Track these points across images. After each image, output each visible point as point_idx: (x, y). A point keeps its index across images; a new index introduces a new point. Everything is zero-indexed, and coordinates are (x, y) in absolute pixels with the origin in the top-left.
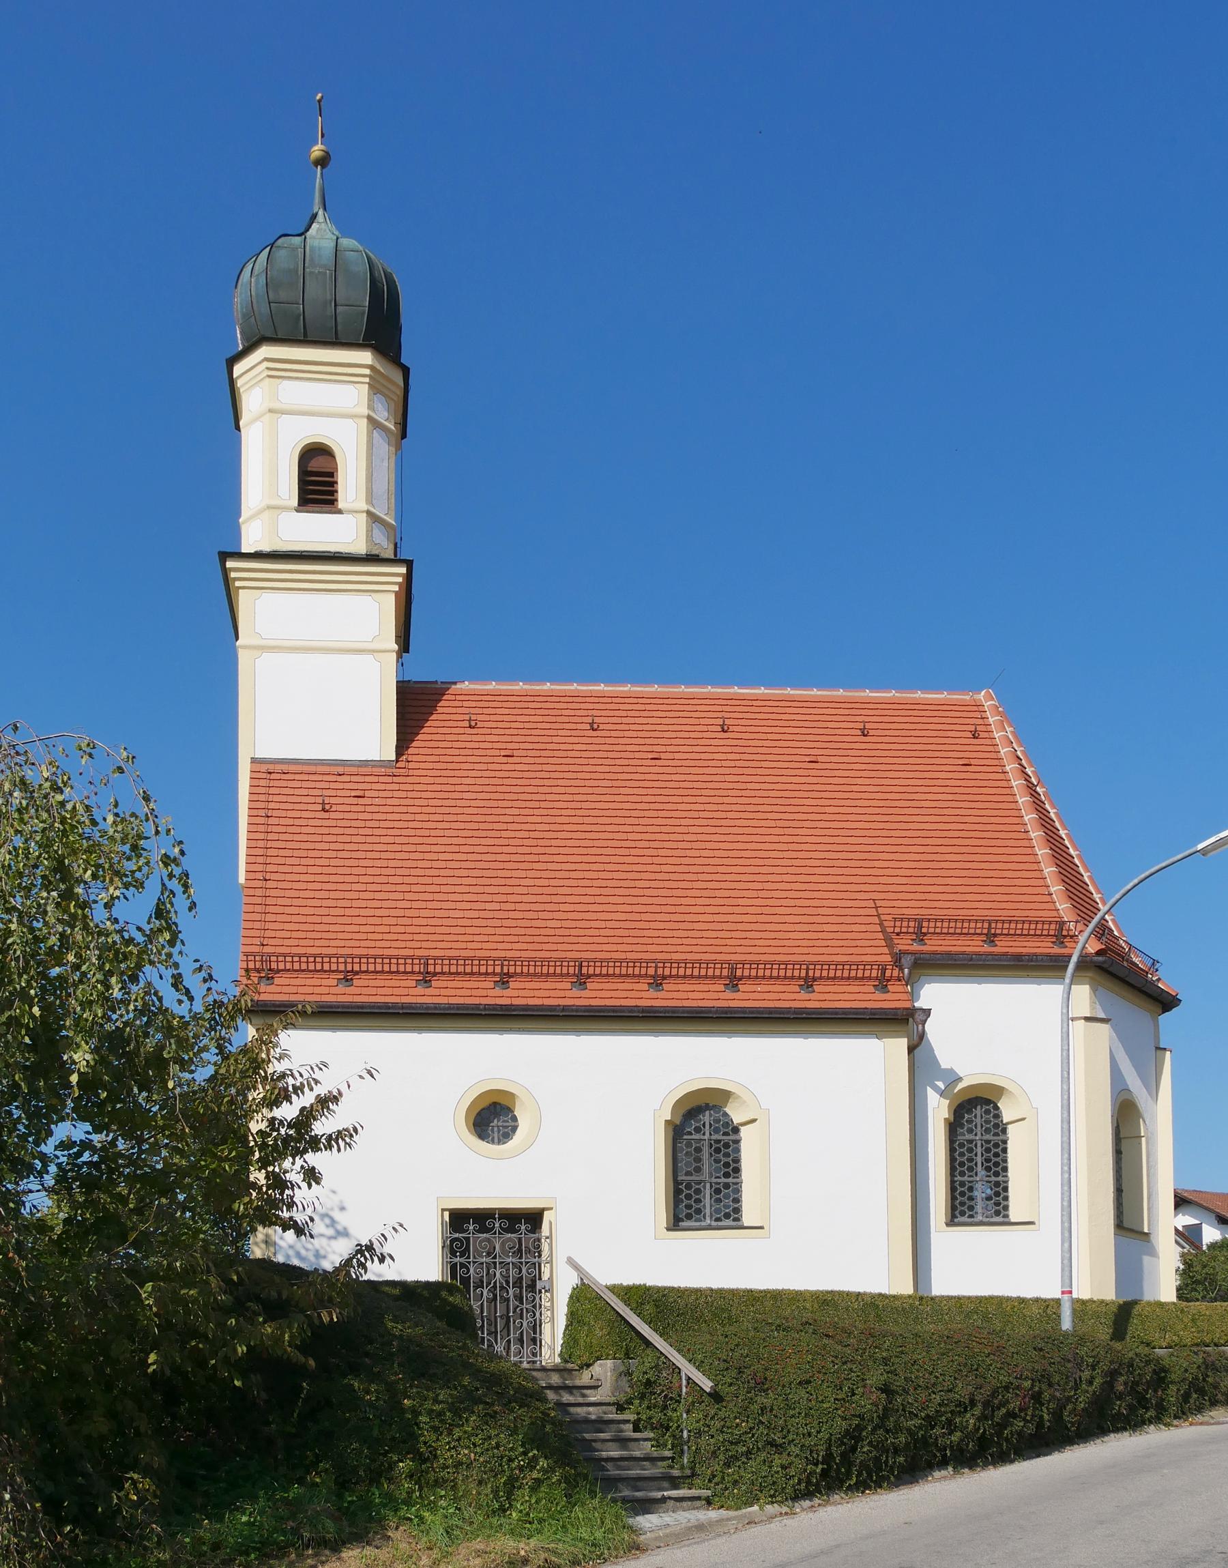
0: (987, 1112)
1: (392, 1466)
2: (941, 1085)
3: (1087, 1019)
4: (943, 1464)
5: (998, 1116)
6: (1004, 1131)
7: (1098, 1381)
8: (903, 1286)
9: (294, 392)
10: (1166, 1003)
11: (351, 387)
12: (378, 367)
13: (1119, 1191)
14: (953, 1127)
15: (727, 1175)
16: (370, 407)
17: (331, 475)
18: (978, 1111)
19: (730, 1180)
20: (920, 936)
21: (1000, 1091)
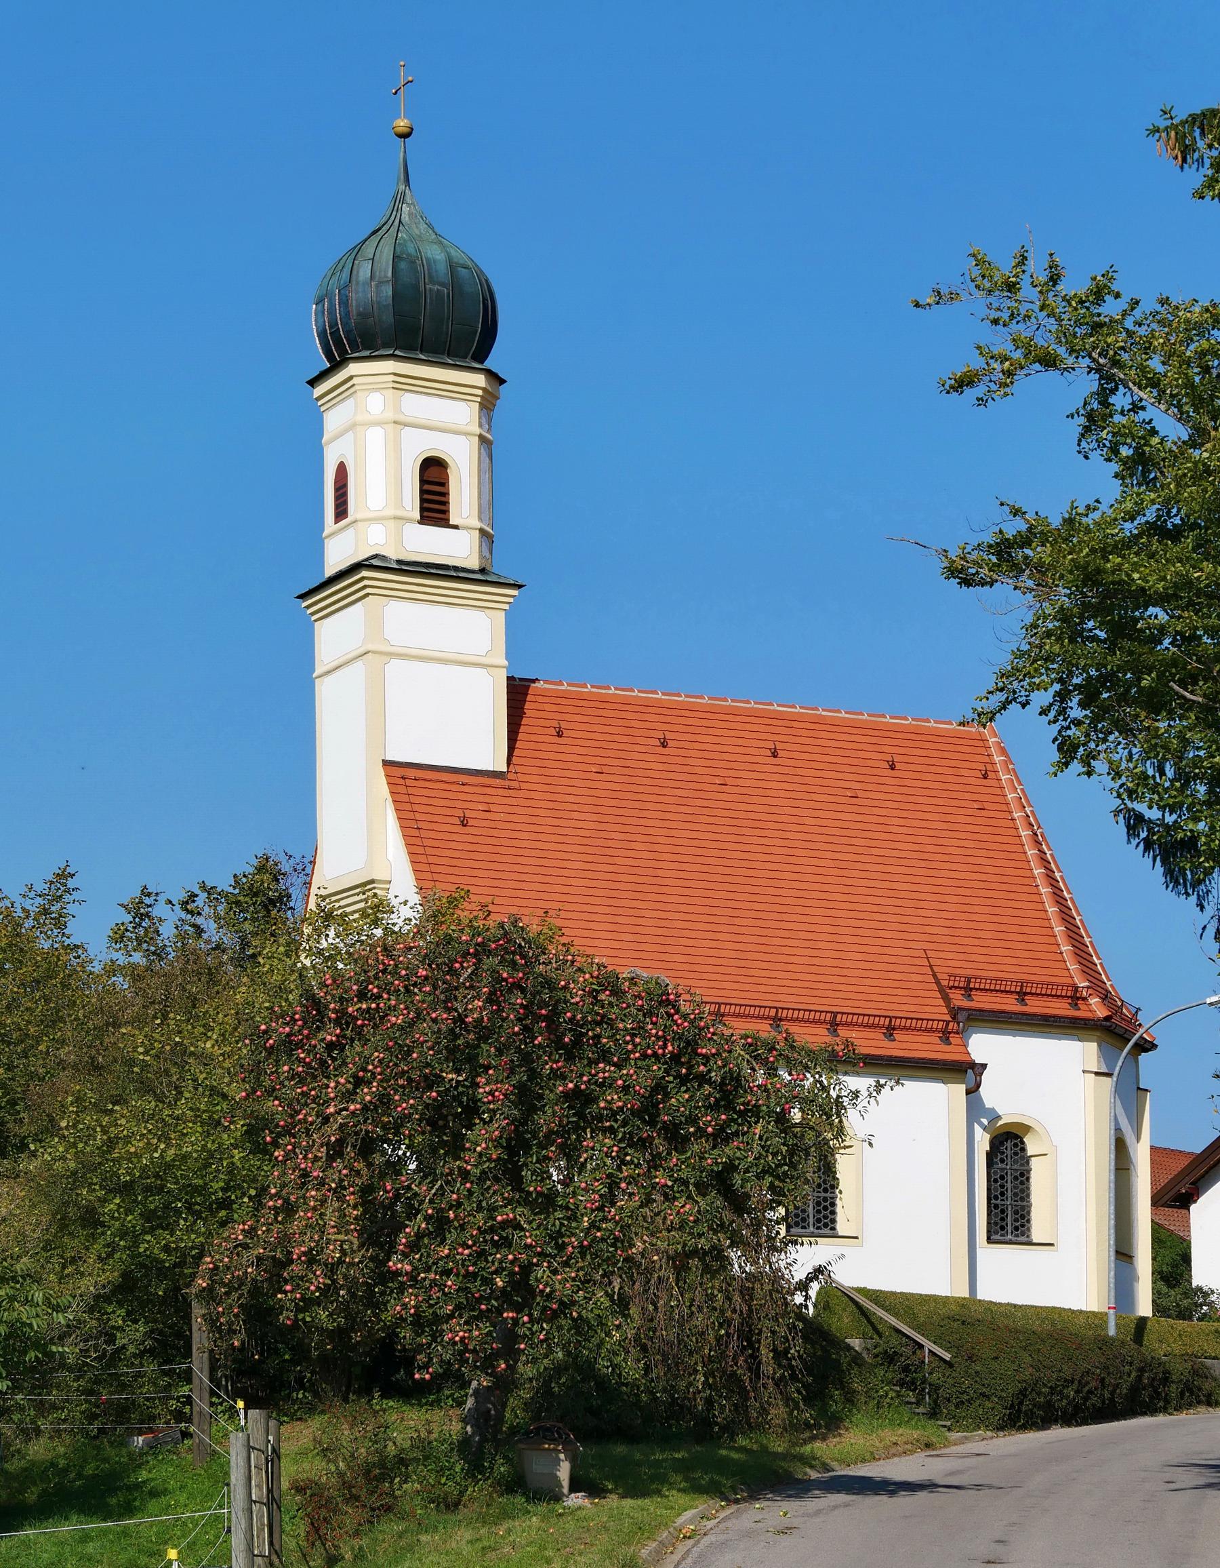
0: (1016, 1145)
2: (985, 1122)
3: (1097, 1074)
4: (1056, 1422)
5: (1023, 1149)
6: (1028, 1162)
7: (1134, 1374)
8: (964, 1293)
9: (417, 406)
10: (1145, 1046)
11: (463, 404)
14: (990, 1156)
15: (826, 1190)
16: (480, 426)
18: (1009, 1144)
19: (828, 1195)
20: (968, 991)
21: (1027, 1129)
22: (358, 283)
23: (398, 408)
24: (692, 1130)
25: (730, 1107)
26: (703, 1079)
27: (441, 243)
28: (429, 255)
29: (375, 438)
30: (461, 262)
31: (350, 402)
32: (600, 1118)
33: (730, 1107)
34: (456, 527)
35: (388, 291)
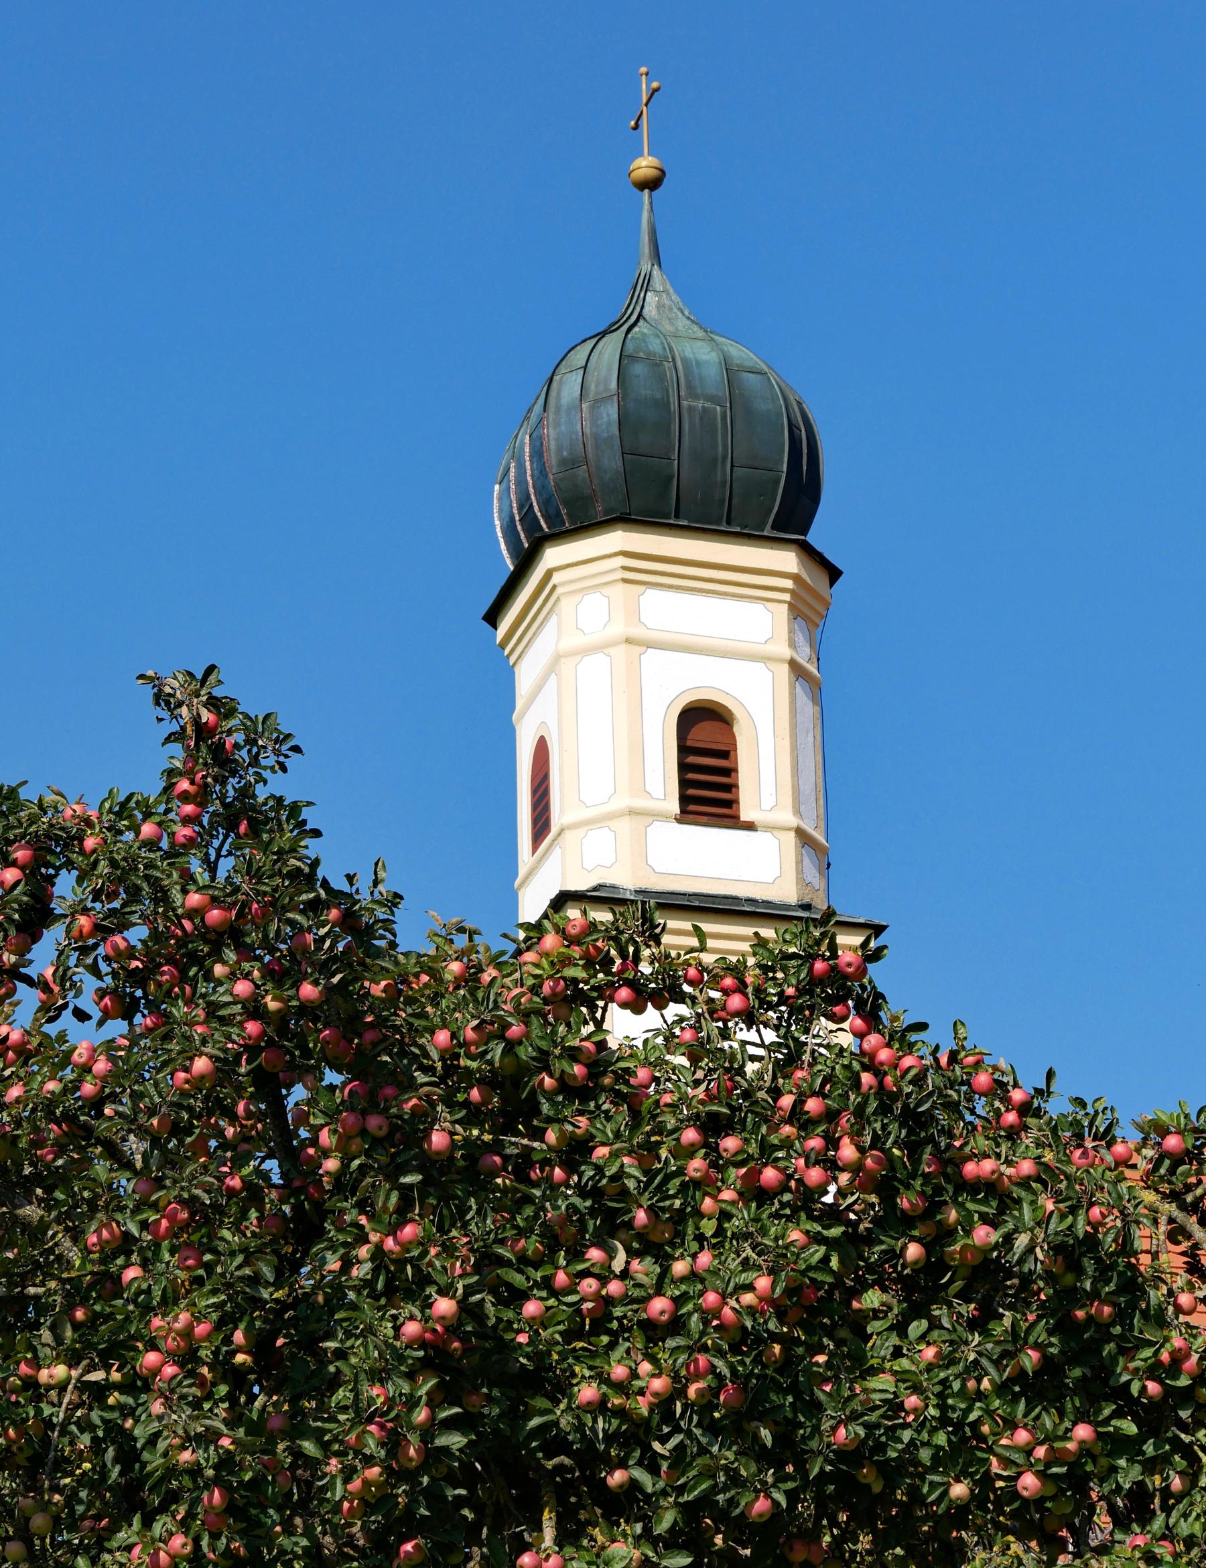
1: (142, 1499)
9: (668, 610)
11: (758, 607)
12: (805, 576)
13: (639, 814)
16: (792, 644)
17: (725, 755)
22: (558, 408)
23: (634, 614)
24: (959, 1490)
25: (1101, 1389)
26: (989, 1279)
27: (712, 339)
28: (688, 353)
29: (594, 677)
30: (748, 364)
31: (554, 619)
32: (592, 1459)
33: (1101, 1389)
34: (750, 826)
35: (611, 412)
